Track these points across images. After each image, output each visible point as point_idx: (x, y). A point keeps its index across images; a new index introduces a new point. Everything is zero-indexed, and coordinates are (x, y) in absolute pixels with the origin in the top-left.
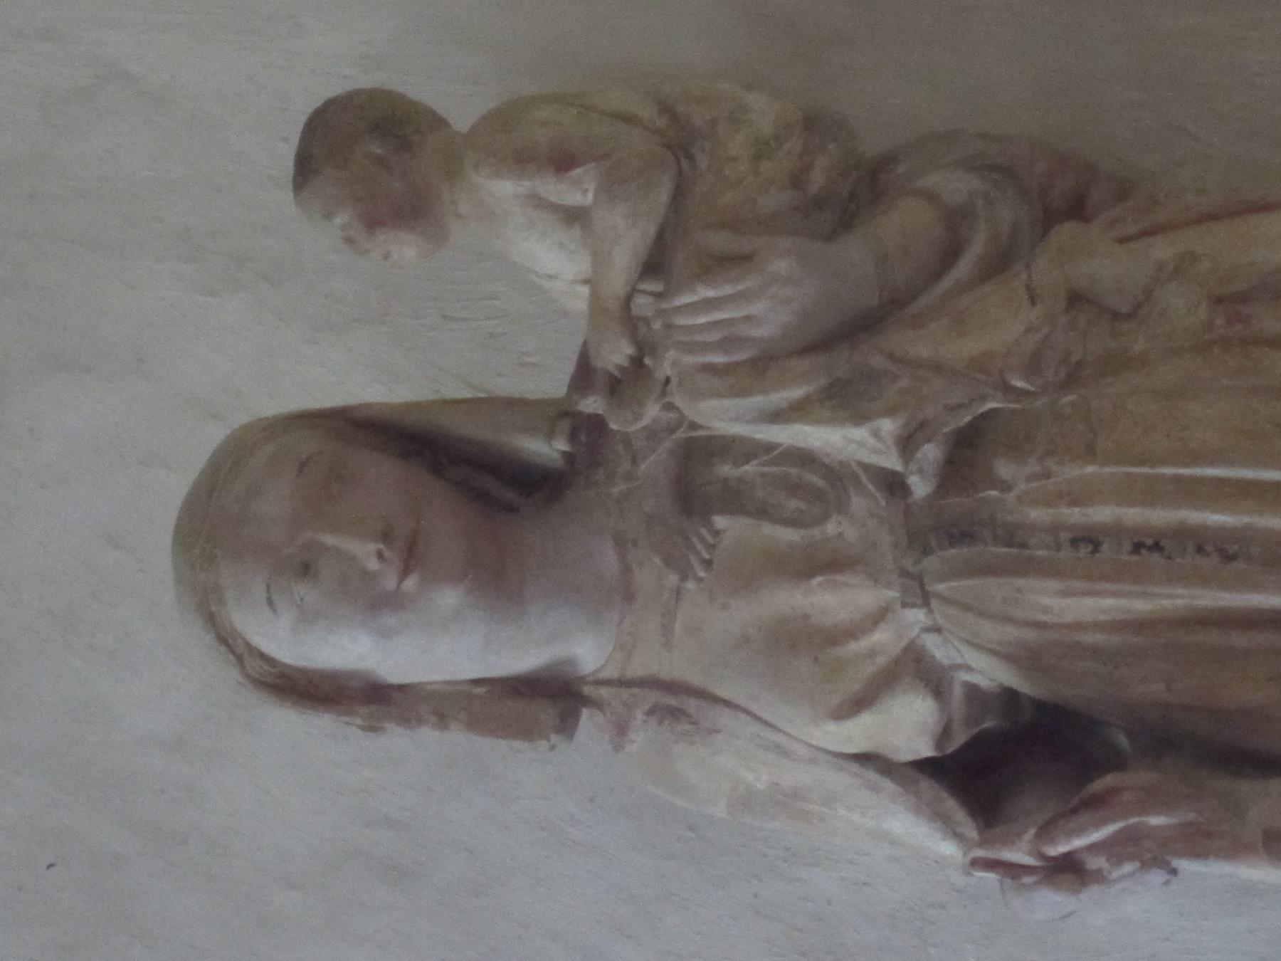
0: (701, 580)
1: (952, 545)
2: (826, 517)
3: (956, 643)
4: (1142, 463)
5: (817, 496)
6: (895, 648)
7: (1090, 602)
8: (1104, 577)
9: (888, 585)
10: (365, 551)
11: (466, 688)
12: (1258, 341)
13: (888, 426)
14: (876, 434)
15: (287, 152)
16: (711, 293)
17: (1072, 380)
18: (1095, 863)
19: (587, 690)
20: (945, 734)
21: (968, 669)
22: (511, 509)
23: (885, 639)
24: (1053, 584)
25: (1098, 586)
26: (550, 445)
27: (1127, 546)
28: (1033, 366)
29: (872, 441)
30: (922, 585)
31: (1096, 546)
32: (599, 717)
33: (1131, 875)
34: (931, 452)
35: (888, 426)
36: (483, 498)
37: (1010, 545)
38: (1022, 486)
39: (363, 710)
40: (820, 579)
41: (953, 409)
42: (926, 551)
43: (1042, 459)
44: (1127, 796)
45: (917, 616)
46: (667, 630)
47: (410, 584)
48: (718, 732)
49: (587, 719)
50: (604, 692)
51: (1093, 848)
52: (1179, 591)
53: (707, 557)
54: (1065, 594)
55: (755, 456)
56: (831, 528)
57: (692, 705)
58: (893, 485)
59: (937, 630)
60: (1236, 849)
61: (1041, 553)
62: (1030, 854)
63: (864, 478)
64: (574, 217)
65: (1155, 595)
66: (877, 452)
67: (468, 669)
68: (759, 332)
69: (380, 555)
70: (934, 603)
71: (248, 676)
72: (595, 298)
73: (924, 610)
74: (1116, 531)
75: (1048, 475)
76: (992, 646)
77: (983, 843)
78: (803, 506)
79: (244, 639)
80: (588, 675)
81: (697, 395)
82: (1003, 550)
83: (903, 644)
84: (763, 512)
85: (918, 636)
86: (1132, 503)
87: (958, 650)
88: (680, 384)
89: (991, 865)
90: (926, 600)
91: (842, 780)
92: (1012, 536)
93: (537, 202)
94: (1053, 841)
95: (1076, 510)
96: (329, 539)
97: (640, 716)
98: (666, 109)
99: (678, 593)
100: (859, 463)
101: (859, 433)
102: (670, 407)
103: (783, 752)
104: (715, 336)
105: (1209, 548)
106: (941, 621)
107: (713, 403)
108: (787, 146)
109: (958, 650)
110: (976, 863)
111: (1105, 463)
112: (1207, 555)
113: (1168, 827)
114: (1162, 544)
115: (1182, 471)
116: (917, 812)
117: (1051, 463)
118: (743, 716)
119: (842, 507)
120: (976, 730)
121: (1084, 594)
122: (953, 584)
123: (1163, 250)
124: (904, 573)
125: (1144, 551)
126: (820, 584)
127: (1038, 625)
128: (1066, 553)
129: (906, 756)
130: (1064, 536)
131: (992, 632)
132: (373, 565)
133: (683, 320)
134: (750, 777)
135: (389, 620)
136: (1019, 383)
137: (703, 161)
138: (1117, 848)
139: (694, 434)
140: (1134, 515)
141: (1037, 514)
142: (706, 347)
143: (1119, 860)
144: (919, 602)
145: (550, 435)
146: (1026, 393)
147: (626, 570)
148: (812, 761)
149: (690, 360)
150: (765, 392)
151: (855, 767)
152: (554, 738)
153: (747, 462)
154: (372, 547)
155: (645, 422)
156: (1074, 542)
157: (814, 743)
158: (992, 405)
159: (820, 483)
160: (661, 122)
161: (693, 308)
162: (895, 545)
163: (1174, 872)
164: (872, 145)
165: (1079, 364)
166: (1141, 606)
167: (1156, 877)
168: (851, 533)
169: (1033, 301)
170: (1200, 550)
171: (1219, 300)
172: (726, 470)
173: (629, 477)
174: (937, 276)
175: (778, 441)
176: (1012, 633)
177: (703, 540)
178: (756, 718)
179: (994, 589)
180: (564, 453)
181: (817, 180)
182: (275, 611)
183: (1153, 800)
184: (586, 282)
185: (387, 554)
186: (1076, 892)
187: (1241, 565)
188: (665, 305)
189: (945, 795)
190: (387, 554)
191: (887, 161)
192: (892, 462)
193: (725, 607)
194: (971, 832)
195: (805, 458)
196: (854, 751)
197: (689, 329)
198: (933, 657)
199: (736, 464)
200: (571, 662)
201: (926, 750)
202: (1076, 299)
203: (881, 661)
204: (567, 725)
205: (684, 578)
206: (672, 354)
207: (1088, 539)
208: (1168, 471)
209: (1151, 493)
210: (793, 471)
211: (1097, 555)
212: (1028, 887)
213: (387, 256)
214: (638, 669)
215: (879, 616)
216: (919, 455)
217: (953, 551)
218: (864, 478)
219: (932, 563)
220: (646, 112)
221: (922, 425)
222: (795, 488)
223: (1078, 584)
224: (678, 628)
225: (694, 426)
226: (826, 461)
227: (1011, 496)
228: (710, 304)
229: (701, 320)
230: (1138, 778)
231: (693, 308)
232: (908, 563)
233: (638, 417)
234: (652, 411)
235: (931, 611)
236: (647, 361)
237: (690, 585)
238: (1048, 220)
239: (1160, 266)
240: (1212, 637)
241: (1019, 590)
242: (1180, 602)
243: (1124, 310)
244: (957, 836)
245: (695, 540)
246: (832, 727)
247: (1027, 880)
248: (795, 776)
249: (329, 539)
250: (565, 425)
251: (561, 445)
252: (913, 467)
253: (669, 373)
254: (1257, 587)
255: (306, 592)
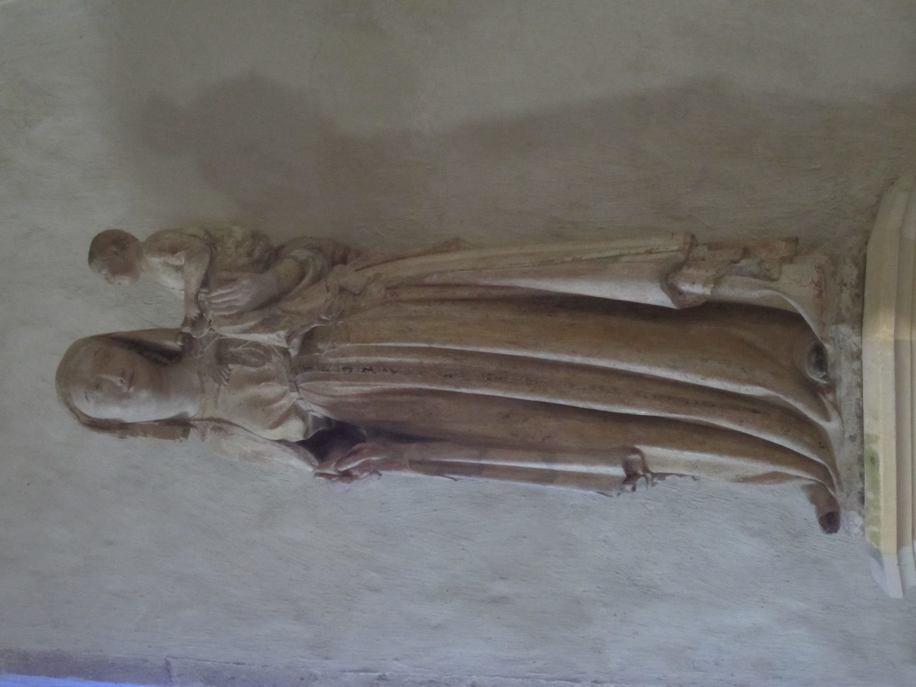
0: (225, 385)
1: (305, 371)
2: (264, 364)
3: (309, 403)
4: (364, 341)
5: (262, 357)
6: (289, 405)
7: (350, 388)
8: (354, 380)
9: (285, 385)
10: (117, 380)
11: (152, 423)
12: (402, 301)
13: (282, 333)
14: (278, 336)
15: (87, 249)
16: (223, 292)
17: (341, 316)
18: (355, 473)
19: (192, 422)
20: (306, 433)
21: (313, 411)
22: (165, 365)
23: (285, 402)
24: (339, 383)
25: (353, 383)
26: (176, 344)
27: (361, 370)
28: (328, 312)
29: (277, 339)
30: (296, 385)
31: (351, 370)
32: (196, 430)
33: (367, 476)
34: (296, 341)
35: (282, 333)
36: (156, 361)
37: (323, 370)
38: (327, 351)
39: (118, 431)
40: (263, 384)
41: (303, 327)
42: (297, 373)
43: (332, 342)
44: (366, 451)
45: (295, 395)
46: (216, 402)
47: (132, 390)
48: (234, 434)
49: (193, 433)
50: (197, 422)
51: (355, 468)
52: (378, 384)
53: (227, 378)
54: (343, 386)
55: (241, 344)
56: (266, 367)
57: (225, 426)
58: (285, 352)
59: (302, 399)
60: (400, 467)
61: (333, 373)
62: (334, 471)
63: (276, 350)
64: (178, 269)
65: (372, 385)
66: (279, 342)
67: (153, 417)
68: (238, 304)
69: (121, 381)
70: (300, 390)
71: (81, 422)
72: (186, 294)
73: (297, 392)
74: (357, 365)
75: (334, 347)
76: (320, 404)
77: (318, 468)
78: (257, 360)
79: (79, 410)
80: (193, 417)
81: (220, 325)
82: (321, 372)
83: (291, 404)
84: (244, 363)
85: (296, 401)
86: (363, 355)
87: (309, 405)
88: (214, 322)
89: (322, 475)
90: (297, 389)
91: (276, 448)
92: (324, 367)
93: (166, 264)
94: (341, 466)
95: (344, 358)
96: (104, 376)
97: (208, 429)
98: (207, 232)
99: (218, 390)
100: (275, 346)
101: (273, 336)
102: (212, 329)
103: (255, 441)
104: (224, 306)
105: (388, 369)
106: (303, 396)
107: (226, 328)
108: (247, 243)
109: (309, 405)
110: (316, 474)
111: (353, 343)
112: (387, 371)
113: (378, 460)
114: (373, 368)
115: (378, 344)
116: (299, 458)
117: (335, 343)
118: (242, 429)
119: (269, 360)
120: (317, 431)
121: (348, 385)
122: (308, 383)
123: (370, 273)
124: (290, 381)
125: (367, 371)
126: (263, 386)
127: (333, 396)
128: (341, 372)
129: (295, 440)
130: (341, 367)
131: (318, 398)
132: (119, 384)
133: (214, 301)
134: (245, 448)
135: (125, 402)
136: (324, 318)
137: (219, 249)
138: (363, 468)
139: (220, 338)
140: (363, 359)
141: (332, 360)
142: (223, 310)
143: (363, 472)
144: (295, 390)
145: (176, 340)
146: (325, 321)
147: (202, 383)
148: (265, 443)
149: (217, 314)
150: (242, 323)
151: (278, 444)
152: (182, 438)
153: (238, 347)
154: (119, 379)
155: (204, 335)
156: (344, 369)
157: (264, 437)
158: (316, 325)
159: (262, 352)
160: (206, 237)
161: (218, 297)
162: (287, 372)
163: (381, 475)
164: (275, 243)
165: (343, 311)
166: (366, 389)
167: (375, 477)
168: (272, 368)
169: (328, 291)
170: (385, 370)
171: (388, 289)
172: (232, 349)
173: (202, 353)
174: (298, 284)
175: (247, 339)
176: (326, 399)
177: (226, 373)
178: (245, 429)
179: (320, 384)
180: (181, 346)
181: (257, 254)
182: (88, 400)
183: (374, 452)
184: (183, 290)
185: (124, 381)
186: (349, 483)
187: (398, 374)
188: (208, 296)
189: (308, 452)
190: (124, 381)
191: (282, 247)
192: (284, 345)
193: (233, 394)
194: (317, 464)
195: (257, 345)
196: (276, 439)
197: (216, 304)
198: (301, 408)
199: (235, 348)
200: (186, 413)
201: (300, 438)
202: (342, 290)
203: (284, 410)
204: (186, 434)
205: (220, 385)
206: (211, 312)
207: (348, 368)
208: (373, 344)
209: (367, 352)
210: (254, 349)
211: (352, 373)
212: (335, 481)
213: (120, 284)
214: (206, 415)
215: (283, 395)
216: (292, 342)
217: (306, 373)
218: (276, 350)
219: (299, 377)
220: (202, 234)
221: (293, 332)
222: (251, 353)
223: (346, 382)
224: (219, 401)
225: (221, 336)
226: (264, 345)
227: (323, 355)
228: (222, 296)
229: (220, 301)
230: (368, 445)
231: (218, 297)
232: (291, 378)
233: (202, 333)
234: (206, 331)
235: (299, 393)
236: (204, 314)
237: (222, 387)
238: (334, 264)
239: (369, 278)
240: (391, 398)
241: (327, 385)
242: (379, 387)
243: (358, 292)
244: (311, 465)
245: (223, 372)
246: (269, 431)
247: (334, 479)
248: (260, 448)
249: (104, 376)
250: (180, 337)
251: (180, 343)
252: (291, 346)
253: (211, 318)
254: (404, 381)
255: (97, 393)
